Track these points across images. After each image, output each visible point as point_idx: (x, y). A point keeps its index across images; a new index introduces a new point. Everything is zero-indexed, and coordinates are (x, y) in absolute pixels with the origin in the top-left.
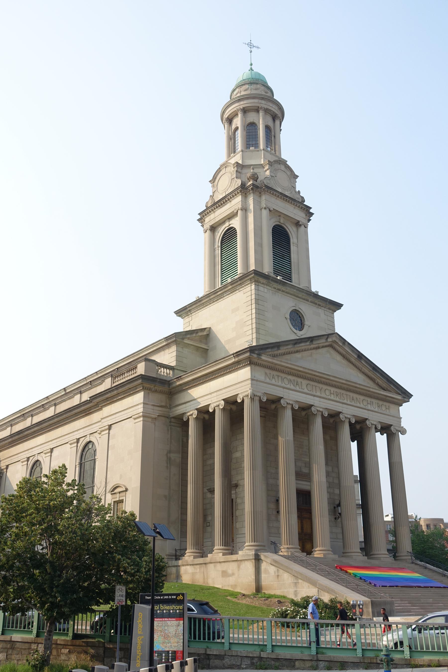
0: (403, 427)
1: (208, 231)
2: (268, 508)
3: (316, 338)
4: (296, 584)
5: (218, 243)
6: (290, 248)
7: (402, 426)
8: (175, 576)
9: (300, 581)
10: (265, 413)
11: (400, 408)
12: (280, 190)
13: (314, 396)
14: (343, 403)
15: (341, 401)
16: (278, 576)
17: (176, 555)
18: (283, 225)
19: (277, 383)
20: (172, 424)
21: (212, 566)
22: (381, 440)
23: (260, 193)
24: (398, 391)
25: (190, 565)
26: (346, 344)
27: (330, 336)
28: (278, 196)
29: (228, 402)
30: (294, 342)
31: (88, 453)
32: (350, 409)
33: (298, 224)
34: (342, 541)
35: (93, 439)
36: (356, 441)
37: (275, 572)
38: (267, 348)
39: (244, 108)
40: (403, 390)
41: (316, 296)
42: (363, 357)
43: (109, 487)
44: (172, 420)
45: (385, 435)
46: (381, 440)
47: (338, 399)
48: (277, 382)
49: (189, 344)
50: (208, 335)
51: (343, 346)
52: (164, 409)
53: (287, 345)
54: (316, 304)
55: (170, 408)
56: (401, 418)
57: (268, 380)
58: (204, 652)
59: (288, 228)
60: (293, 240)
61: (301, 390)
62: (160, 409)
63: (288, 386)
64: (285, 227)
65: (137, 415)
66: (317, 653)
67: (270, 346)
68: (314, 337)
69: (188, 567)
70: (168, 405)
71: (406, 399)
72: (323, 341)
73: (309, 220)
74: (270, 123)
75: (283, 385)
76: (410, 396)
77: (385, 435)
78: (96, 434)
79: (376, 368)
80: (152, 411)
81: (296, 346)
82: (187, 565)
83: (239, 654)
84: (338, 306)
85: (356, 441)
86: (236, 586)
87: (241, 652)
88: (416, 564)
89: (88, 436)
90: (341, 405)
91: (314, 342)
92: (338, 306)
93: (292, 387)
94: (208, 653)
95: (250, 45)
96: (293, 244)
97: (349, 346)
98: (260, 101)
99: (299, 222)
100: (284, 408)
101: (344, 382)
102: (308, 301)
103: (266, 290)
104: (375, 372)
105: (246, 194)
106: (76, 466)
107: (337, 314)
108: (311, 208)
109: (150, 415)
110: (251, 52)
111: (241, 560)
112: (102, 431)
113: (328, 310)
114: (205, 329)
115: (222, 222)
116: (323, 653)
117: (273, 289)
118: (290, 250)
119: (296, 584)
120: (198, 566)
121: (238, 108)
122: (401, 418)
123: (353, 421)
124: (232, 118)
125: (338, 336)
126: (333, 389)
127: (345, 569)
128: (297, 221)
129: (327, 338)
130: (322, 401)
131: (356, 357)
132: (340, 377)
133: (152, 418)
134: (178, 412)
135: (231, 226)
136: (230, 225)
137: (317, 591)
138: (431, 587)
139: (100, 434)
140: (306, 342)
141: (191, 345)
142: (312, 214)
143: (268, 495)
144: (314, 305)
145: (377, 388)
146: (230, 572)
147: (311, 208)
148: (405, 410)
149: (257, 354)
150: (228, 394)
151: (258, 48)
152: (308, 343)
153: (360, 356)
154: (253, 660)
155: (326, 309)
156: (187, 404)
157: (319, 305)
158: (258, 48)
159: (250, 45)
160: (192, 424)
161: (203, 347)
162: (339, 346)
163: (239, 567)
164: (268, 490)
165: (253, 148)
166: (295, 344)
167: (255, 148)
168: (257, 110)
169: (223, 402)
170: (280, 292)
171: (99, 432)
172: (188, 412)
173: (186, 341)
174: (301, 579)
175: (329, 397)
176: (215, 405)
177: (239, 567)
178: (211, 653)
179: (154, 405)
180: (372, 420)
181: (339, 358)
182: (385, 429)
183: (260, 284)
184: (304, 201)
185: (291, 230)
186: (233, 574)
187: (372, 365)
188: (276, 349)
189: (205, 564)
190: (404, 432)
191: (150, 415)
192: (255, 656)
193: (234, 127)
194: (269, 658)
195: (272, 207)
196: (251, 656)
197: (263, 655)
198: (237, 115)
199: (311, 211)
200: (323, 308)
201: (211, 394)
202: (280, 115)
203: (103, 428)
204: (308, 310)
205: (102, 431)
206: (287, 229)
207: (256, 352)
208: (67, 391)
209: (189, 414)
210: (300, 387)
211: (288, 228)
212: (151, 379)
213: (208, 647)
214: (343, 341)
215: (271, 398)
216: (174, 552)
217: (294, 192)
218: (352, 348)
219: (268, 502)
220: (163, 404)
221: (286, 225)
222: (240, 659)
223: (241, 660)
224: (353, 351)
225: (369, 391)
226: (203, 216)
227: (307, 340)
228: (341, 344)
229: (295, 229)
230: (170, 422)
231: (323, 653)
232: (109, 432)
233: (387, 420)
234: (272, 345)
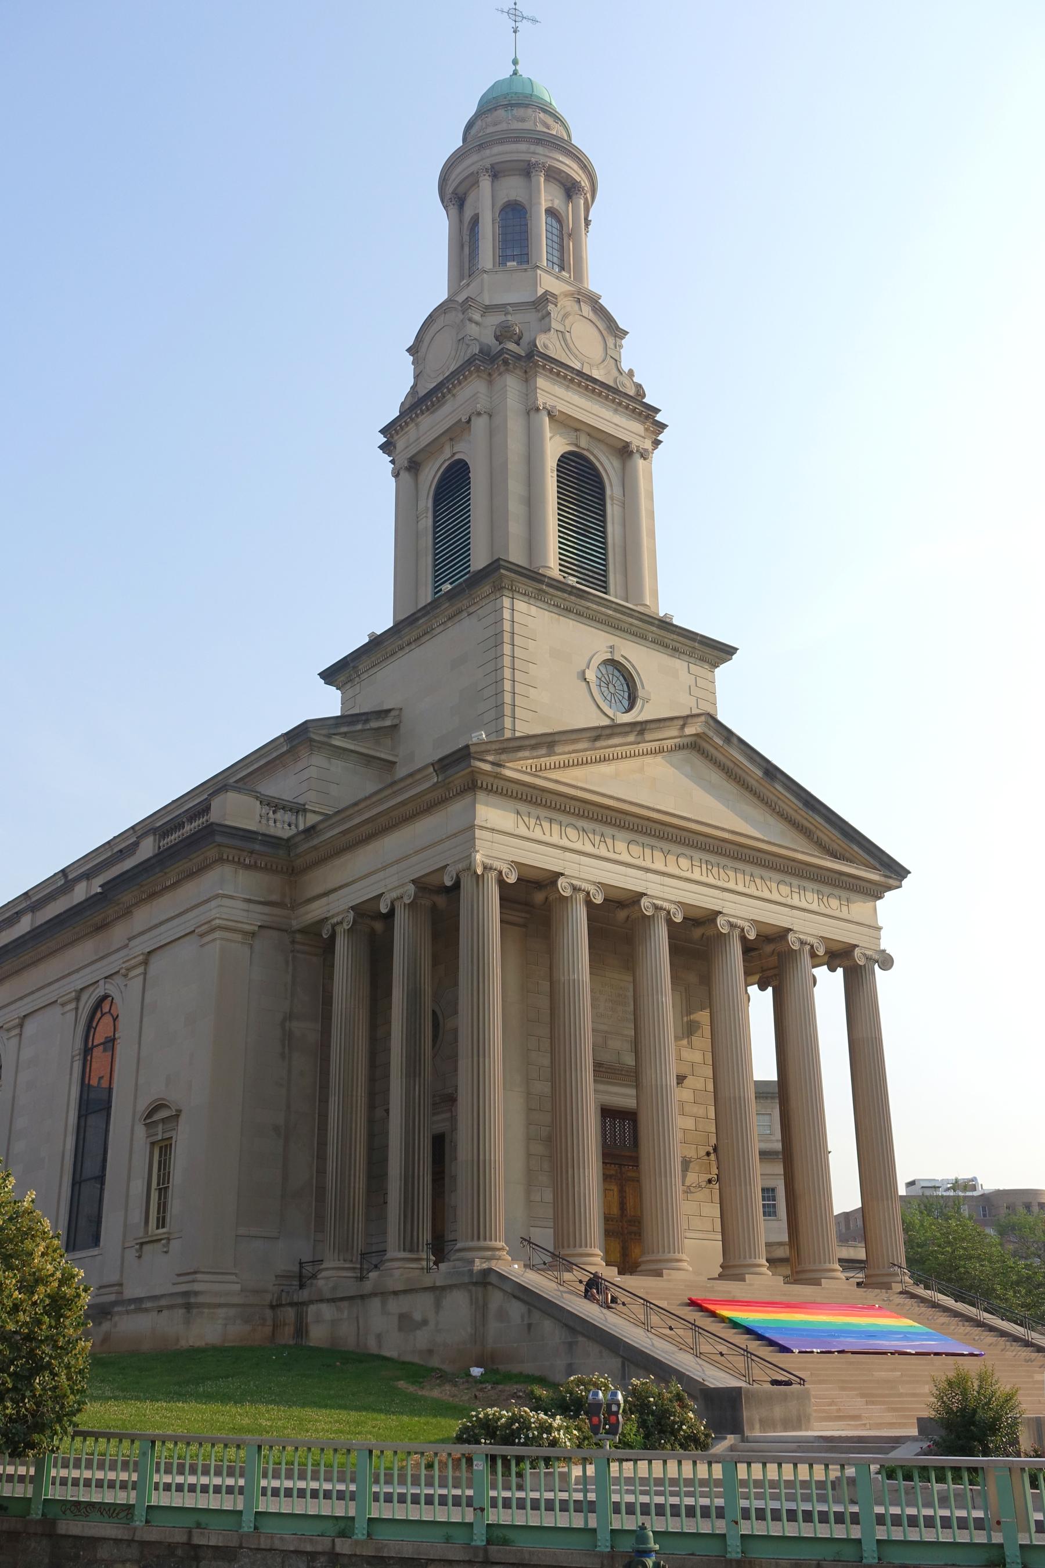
0: (884, 951)
1: (402, 473)
2: (529, 1155)
3: (653, 726)
4: (571, 1346)
5: (427, 503)
6: (604, 511)
7: (882, 947)
8: (292, 1328)
9: (580, 1339)
10: (523, 915)
11: (879, 903)
12: (577, 366)
13: (648, 870)
14: (648, 870)
15: (720, 884)
16: (529, 1326)
17: (301, 1276)
19: (547, 838)
20: (298, 947)
21: (376, 1303)
22: (828, 988)
23: (526, 372)
24: (872, 861)
25: (328, 1301)
26: (735, 741)
27: (690, 720)
28: (572, 380)
29: (425, 888)
30: (594, 734)
31: (101, 1024)
32: (744, 902)
33: (624, 452)
34: (720, 1237)
35: (111, 989)
36: (770, 989)
37: (522, 1317)
38: (520, 748)
39: (492, 166)
40: (886, 860)
41: (666, 625)
42: (779, 776)
43: (143, 1105)
44: (299, 937)
45: (840, 971)
46: (828, 988)
47: (711, 880)
48: (548, 833)
49: (345, 750)
50: (395, 727)
51: (726, 747)
52: (276, 911)
53: (575, 741)
54: (667, 647)
55: (293, 908)
56: (880, 929)
58: (184, 1539)
60: (613, 491)
61: (611, 855)
62: (267, 909)
63: (578, 846)
64: (592, 458)
65: (206, 926)
66: (489, 1542)
67: (527, 742)
68: (647, 722)
69: (324, 1307)
70: (287, 900)
71: (891, 882)
72: (674, 732)
73: (657, 443)
74: (558, 203)
75: (565, 842)
76: (903, 873)
77: (840, 971)
78: (118, 980)
79: (813, 802)
80: (245, 914)
81: (598, 744)
82: (321, 1301)
83: (278, 1544)
84: (726, 652)
85: (770, 989)
86: (430, 1352)
87: (282, 1539)
88: (913, 1296)
89: (102, 983)
91: (648, 736)
92: (726, 652)
94: (197, 1540)
95: (515, 14)
96: (612, 499)
97: (743, 747)
98: (533, 148)
99: (627, 445)
100: (564, 899)
101: (726, 835)
102: (644, 638)
104: (811, 813)
105: (490, 375)
106: (73, 1057)
107: (723, 672)
108: (657, 411)
109: (240, 925)
111: (443, 1288)
112: (128, 970)
113: (698, 662)
114: (390, 711)
115: (432, 449)
116: (505, 1542)
117: (552, 608)
118: (604, 516)
119: (571, 1346)
120: (346, 1304)
122: (880, 929)
123: (752, 936)
124: (465, 194)
125: (711, 722)
127: (711, 1307)
128: (623, 444)
129: (683, 726)
130: (670, 883)
131: (759, 773)
132: (720, 825)
133: (245, 933)
134: (310, 916)
135: (456, 457)
136: (454, 454)
137: (620, 1365)
138: (936, 1354)
139: (125, 976)
140: (626, 734)
141: (352, 751)
142: (663, 426)
143: (529, 1124)
144: (661, 648)
145: (816, 854)
146: (417, 1316)
147: (657, 411)
148: (889, 907)
150: (420, 868)
151: (534, 21)
152: (631, 738)
153: (772, 772)
154: (313, 1560)
155: (692, 660)
156: (333, 897)
157: (675, 649)
158: (534, 21)
159: (515, 14)
160: (342, 946)
161: (383, 756)
163: (438, 1306)
164: (530, 1110)
165: (515, 263)
166: (597, 738)
167: (520, 263)
169: (411, 888)
170: (572, 616)
171: (123, 971)
172: (333, 916)
173: (337, 742)
174: (584, 1335)
175: (688, 875)
176: (394, 895)
177: (438, 1306)
178: (203, 1542)
179: (249, 901)
182: (839, 956)
183: (516, 595)
184: (644, 396)
185: (607, 466)
186: (425, 1322)
187: (803, 795)
188: (543, 751)
189: (362, 1297)
190: (887, 962)
191: (240, 925)
192: (319, 1549)
193: (468, 214)
194: (355, 1555)
196: (309, 1548)
197: (343, 1547)
198: (476, 183)
199: (659, 417)
200: (686, 658)
201: (384, 868)
202: (585, 183)
203: (133, 962)
204: (644, 660)
205: (128, 970)
207: (490, 758)
208: (70, 877)
209: (334, 920)
210: (611, 849)
212: (241, 833)
213: (199, 1526)
214: (725, 733)
215: (692, 914)
216: (296, 1269)
217: (615, 373)
218: (749, 752)
219: (529, 1139)
220: (274, 898)
221: (595, 452)
222: (279, 1560)
223: (283, 1562)
224: (752, 760)
225: (794, 860)
226: (392, 436)
227: (628, 729)
229: (617, 463)
230: (293, 942)
231: (505, 1542)
232: (145, 970)
233: (844, 934)
234: (533, 742)
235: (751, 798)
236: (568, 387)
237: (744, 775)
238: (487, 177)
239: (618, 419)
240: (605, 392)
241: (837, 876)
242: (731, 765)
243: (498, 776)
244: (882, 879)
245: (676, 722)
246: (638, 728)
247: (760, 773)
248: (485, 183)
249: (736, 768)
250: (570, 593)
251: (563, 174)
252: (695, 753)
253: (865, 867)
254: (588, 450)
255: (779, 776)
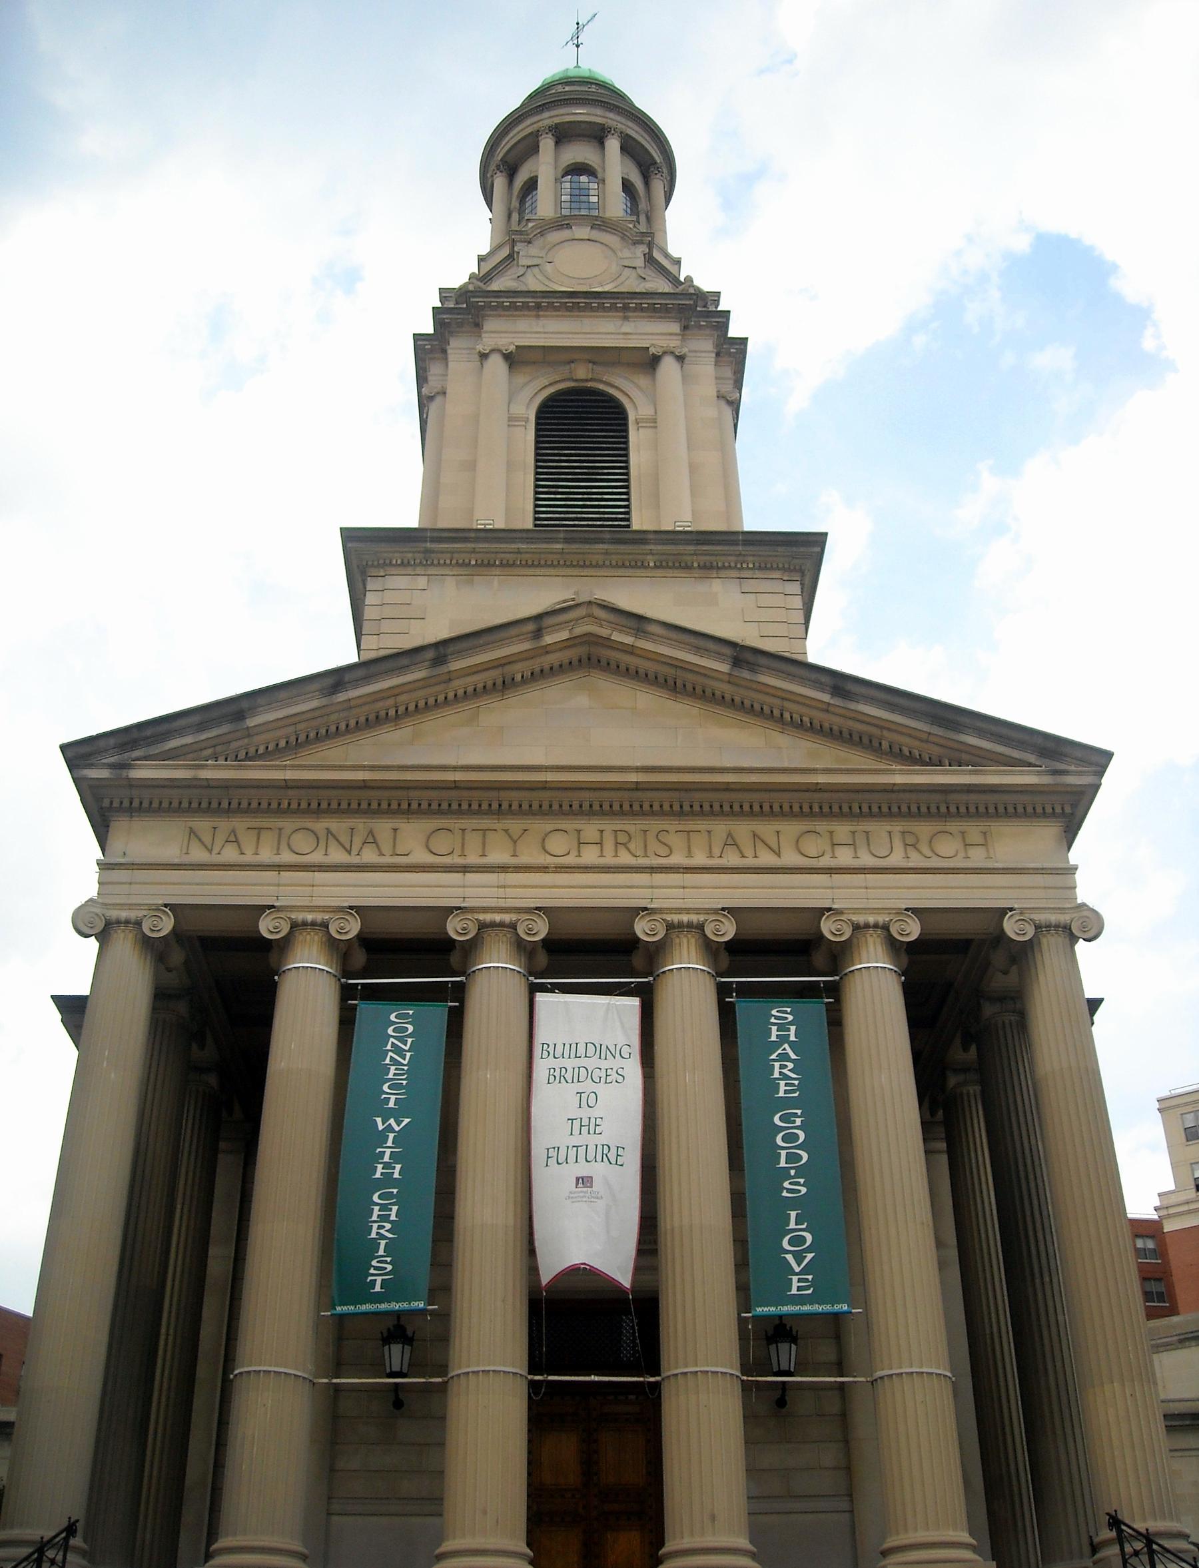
0: (1084, 905)
7: (1079, 901)
13: (465, 869)
18: (589, 384)
24: (1016, 754)
28: (538, 307)
30: (329, 681)
54: (688, 567)
56: (1075, 868)
57: (198, 854)
59: (613, 386)
63: (317, 857)
64: (601, 387)
75: (287, 857)
90: (643, 878)
91: (456, 665)
93: (337, 856)
103: (422, 582)
108: (417, 337)
110: (578, 46)
121: (620, 126)
126: (590, 829)
129: (538, 634)
149: (112, 766)
162: (630, 650)
168: (598, 135)
175: (571, 860)
180: (856, 911)
181: (646, 698)
195: (508, 342)
198: (534, 149)
206: (611, 391)
211: (613, 386)
228: (628, 640)
235: (730, 713)
236: (538, 317)
237: (700, 680)
238: (550, 135)
239: (627, 327)
240: (544, 302)
241: (938, 797)
242: (670, 672)
243: (132, 784)
244: (1046, 780)
245: (514, 631)
246: (430, 654)
247: (724, 668)
248: (547, 144)
249: (679, 673)
250: (476, 540)
251: (583, 126)
252: (604, 683)
253: (1054, 781)
254: (591, 380)
255: (763, 661)
